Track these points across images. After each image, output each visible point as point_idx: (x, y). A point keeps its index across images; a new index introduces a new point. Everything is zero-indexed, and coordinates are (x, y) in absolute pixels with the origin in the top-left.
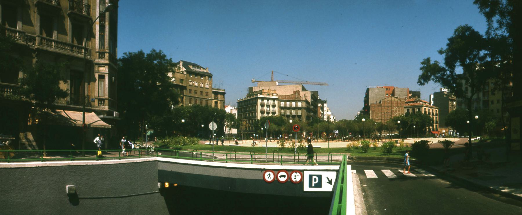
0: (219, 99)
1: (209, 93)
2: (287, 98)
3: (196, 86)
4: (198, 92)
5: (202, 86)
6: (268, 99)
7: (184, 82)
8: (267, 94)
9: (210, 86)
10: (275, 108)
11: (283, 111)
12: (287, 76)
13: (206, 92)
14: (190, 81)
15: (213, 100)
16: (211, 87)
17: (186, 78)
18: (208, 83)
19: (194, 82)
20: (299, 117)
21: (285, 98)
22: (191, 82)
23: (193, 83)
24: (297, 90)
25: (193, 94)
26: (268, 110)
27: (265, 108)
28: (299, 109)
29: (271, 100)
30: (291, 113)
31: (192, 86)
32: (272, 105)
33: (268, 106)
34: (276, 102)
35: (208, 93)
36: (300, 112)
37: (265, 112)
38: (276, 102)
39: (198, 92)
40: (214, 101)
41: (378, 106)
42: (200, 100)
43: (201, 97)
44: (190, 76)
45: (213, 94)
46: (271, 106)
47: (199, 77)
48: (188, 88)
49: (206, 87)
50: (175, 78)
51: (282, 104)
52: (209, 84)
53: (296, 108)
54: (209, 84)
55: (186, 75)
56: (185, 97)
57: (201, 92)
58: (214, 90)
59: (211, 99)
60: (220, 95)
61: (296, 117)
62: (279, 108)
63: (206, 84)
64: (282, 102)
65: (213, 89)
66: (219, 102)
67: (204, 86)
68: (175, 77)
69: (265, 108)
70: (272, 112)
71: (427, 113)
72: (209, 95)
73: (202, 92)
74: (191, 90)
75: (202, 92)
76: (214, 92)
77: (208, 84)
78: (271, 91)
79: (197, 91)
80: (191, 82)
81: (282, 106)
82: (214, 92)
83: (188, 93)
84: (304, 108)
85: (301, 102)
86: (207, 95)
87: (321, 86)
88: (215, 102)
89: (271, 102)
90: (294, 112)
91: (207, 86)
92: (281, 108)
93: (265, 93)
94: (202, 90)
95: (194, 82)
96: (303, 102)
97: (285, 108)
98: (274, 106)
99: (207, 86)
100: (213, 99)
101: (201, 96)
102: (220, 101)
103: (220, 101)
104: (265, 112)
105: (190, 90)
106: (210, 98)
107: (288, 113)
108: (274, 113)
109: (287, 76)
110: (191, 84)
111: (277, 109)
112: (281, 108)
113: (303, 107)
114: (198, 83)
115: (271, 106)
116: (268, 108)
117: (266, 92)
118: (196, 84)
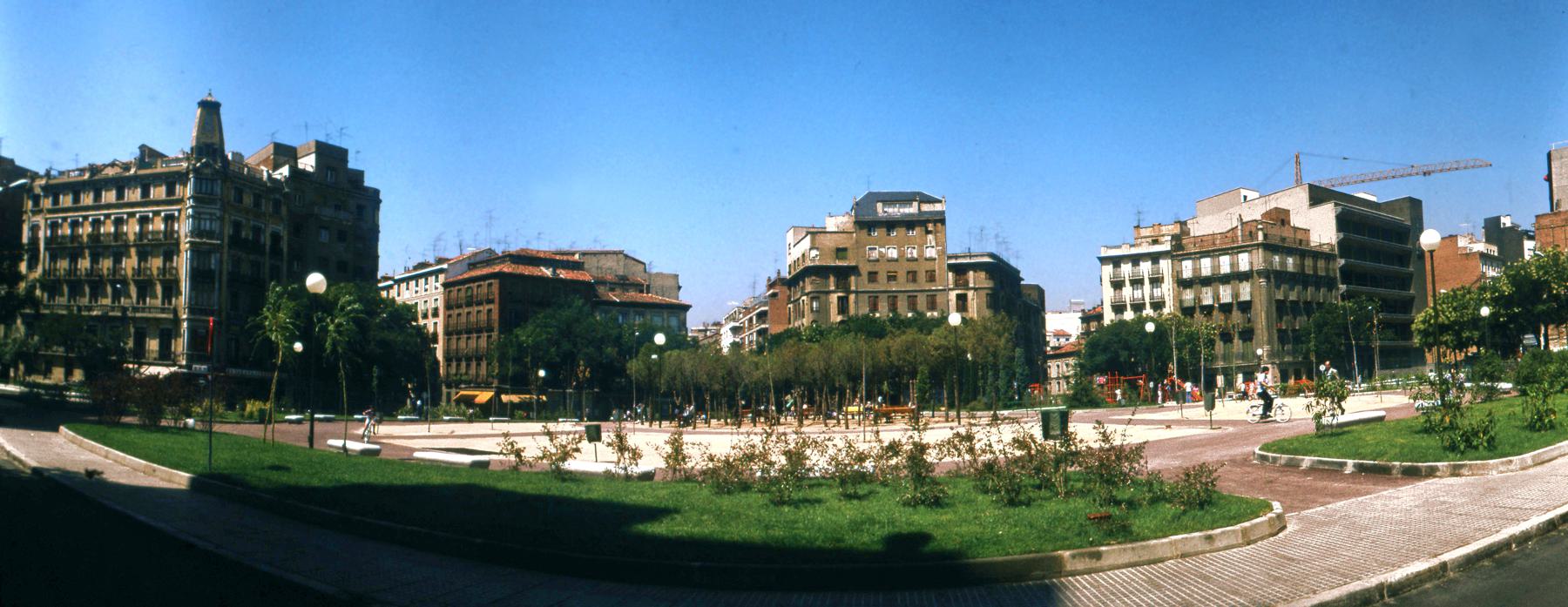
0: (971, 285)
1: (937, 271)
2: (1218, 242)
3: (892, 260)
4: (902, 276)
5: (915, 255)
6: (1135, 260)
7: (850, 254)
8: (1150, 240)
9: (938, 252)
10: (1163, 285)
11: (1188, 296)
12: (1345, 159)
13: (927, 272)
14: (870, 249)
15: (832, 295)
16: (942, 253)
17: (857, 242)
18: (933, 244)
19: (883, 250)
20: (1245, 307)
21: (1214, 244)
22: (875, 249)
23: (880, 252)
24: (1272, 207)
25: (882, 285)
26: (1140, 296)
27: (1127, 292)
28: (1241, 281)
29: (1128, 263)
30: (1216, 297)
31: (878, 261)
32: (1130, 280)
33: (1137, 282)
34: (1165, 265)
35: (934, 271)
36: (1245, 291)
37: (1129, 307)
38: (1165, 265)
39: (902, 276)
40: (953, 295)
41: (1562, 220)
42: (909, 297)
43: (911, 289)
44: (870, 235)
45: (950, 274)
46: (1147, 282)
47: (902, 231)
48: (865, 269)
49: (928, 255)
50: (817, 249)
51: (1187, 270)
52: (937, 245)
53: (1237, 277)
54: (937, 245)
55: (854, 235)
56: (852, 297)
57: (908, 272)
58: (953, 261)
59: (945, 290)
60: (975, 271)
61: (1235, 308)
62: (1176, 285)
63: (927, 247)
64: (1222, 258)
65: (950, 257)
66: (970, 294)
67: (921, 252)
68: (817, 246)
69: (1127, 292)
70: (1151, 304)
71: (166, 301)
72: (937, 279)
73: (913, 276)
74: (876, 273)
75: (913, 276)
76: (952, 268)
77: (933, 247)
78: (1163, 228)
79: (896, 272)
80: (875, 249)
81: (1185, 276)
82: (952, 268)
83: (866, 282)
84: (1260, 273)
85: (1250, 252)
86: (931, 277)
87: (1427, 177)
88: (958, 296)
89: (1146, 267)
90: (1226, 294)
91: (930, 253)
92: (1183, 284)
93: (1143, 240)
94: (913, 266)
95: (883, 250)
96: (1255, 251)
97: (1199, 281)
98: (1156, 281)
99: (931, 253)
100: (951, 286)
101: (911, 284)
102: (975, 289)
103: (975, 289)
104: (1129, 307)
105: (870, 273)
106: (940, 288)
107: (1208, 301)
108: (1158, 305)
109: (1345, 159)
110: (875, 255)
111: (1167, 290)
112: (1183, 284)
113: (1255, 269)
114: (899, 248)
115: (1147, 282)
116: (1140, 291)
117: (1148, 234)
118: (893, 253)
